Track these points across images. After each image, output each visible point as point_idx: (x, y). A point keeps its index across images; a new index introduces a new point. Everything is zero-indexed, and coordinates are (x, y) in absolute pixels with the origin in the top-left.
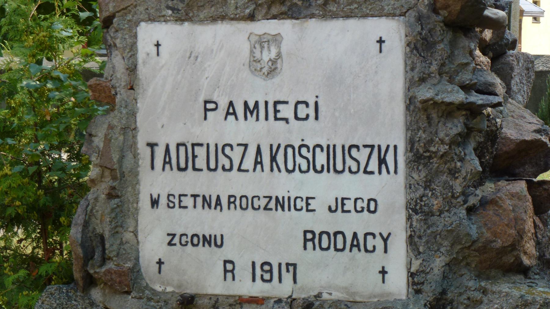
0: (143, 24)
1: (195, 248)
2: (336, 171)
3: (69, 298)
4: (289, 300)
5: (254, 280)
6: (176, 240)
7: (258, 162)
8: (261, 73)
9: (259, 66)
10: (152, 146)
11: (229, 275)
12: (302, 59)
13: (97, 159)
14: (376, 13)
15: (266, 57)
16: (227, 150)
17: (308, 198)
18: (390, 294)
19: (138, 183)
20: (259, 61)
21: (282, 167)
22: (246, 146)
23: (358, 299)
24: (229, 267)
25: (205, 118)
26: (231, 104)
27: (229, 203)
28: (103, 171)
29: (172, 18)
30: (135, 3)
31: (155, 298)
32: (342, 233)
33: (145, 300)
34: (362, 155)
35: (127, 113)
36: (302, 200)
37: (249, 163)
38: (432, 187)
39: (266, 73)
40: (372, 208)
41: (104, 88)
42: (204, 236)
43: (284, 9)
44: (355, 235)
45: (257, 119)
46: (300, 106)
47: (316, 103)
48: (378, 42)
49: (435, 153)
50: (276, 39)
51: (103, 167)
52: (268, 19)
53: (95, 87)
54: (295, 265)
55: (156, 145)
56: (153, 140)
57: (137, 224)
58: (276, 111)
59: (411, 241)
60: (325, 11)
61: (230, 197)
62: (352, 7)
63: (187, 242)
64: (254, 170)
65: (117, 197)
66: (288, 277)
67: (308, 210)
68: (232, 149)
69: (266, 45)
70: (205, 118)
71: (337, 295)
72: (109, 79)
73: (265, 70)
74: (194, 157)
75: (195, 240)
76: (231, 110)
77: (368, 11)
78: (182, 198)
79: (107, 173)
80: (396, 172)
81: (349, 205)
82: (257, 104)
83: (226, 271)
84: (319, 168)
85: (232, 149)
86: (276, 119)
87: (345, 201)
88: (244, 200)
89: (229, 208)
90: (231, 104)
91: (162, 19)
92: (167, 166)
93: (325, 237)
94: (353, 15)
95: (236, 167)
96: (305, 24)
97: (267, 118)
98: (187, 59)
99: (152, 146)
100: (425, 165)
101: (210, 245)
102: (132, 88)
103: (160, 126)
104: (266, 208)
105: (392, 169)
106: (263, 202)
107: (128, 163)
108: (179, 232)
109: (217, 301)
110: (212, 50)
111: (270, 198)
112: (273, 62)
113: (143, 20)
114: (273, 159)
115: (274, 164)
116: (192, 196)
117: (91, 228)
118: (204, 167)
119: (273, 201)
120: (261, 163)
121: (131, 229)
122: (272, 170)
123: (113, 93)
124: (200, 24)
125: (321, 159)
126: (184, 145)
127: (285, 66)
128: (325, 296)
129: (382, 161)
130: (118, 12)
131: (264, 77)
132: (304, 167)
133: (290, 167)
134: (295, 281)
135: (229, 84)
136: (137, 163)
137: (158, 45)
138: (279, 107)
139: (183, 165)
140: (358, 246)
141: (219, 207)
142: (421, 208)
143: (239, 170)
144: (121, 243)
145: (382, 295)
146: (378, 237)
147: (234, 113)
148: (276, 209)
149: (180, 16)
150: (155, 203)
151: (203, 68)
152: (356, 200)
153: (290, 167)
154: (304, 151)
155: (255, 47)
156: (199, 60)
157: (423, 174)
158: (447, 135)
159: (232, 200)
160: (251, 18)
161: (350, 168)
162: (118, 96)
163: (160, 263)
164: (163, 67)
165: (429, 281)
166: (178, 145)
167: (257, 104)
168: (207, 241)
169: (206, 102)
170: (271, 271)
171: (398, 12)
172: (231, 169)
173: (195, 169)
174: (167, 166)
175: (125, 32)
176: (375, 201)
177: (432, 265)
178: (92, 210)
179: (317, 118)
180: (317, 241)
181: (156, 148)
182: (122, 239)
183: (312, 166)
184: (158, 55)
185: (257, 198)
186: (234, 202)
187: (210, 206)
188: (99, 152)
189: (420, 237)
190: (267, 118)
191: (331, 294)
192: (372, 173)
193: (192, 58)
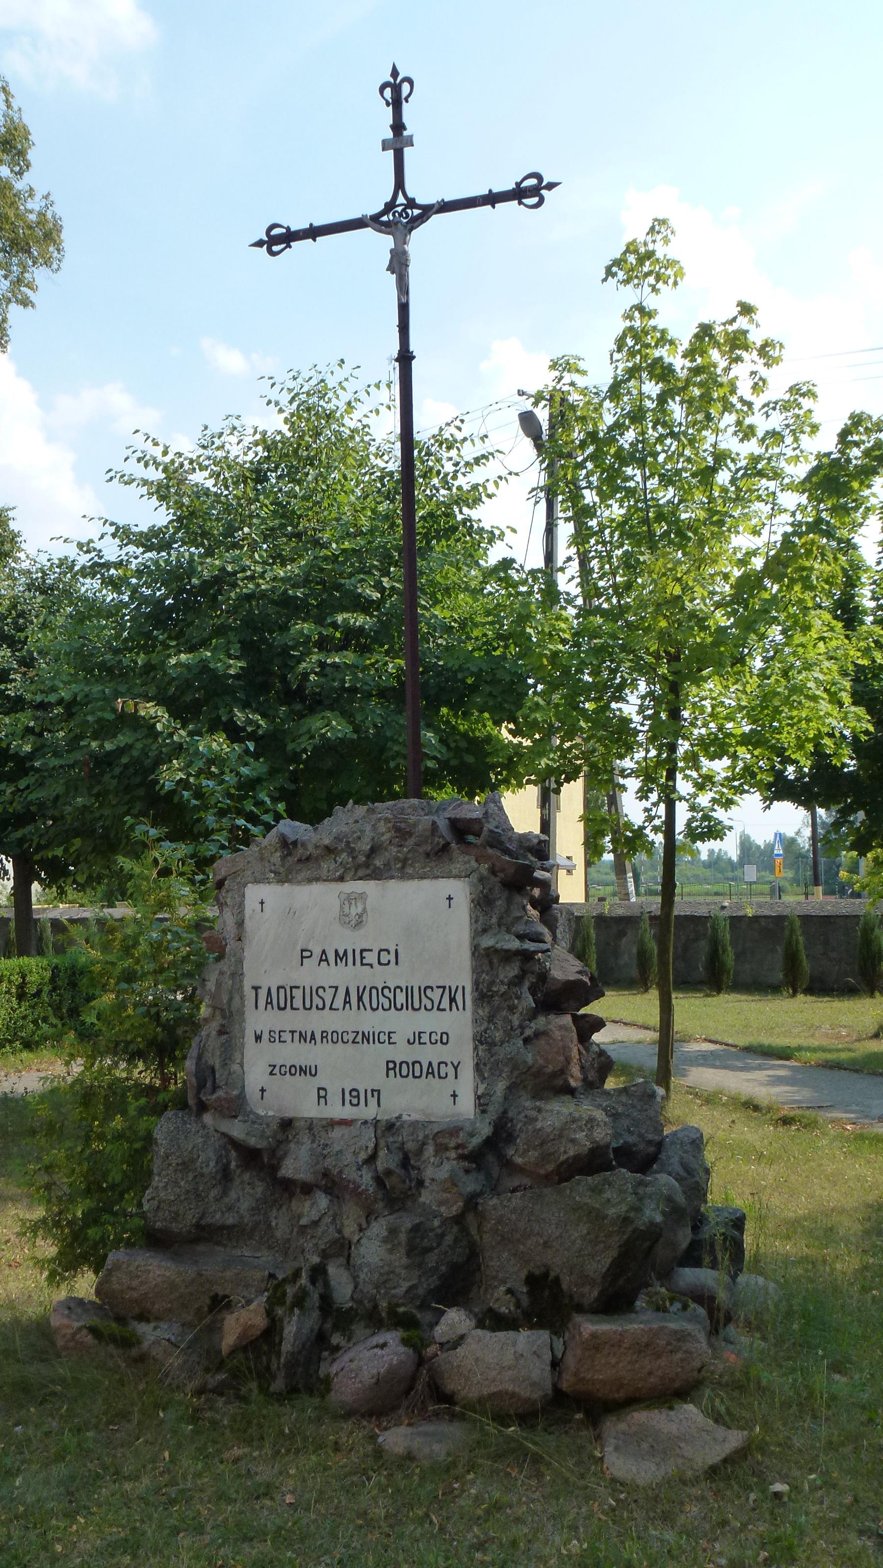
3: (185, 1123)
5: (343, 1104)
6: (277, 1071)
7: (347, 1002)
9: (347, 920)
10: (256, 989)
11: (322, 1100)
15: (354, 912)
16: (321, 991)
19: (244, 1021)
22: (336, 988)
23: (433, 1119)
24: (322, 1093)
26: (324, 952)
27: (322, 1037)
34: (436, 995)
37: (339, 1002)
40: (445, 1040)
43: (368, 872)
44: (430, 1064)
50: (362, 896)
51: (215, 1008)
59: (477, 1068)
61: (323, 1032)
66: (372, 1102)
71: (415, 1117)
73: (353, 923)
74: (292, 998)
76: (323, 958)
79: (218, 1013)
81: (425, 1038)
82: (345, 952)
83: (319, 1097)
84: (399, 1006)
86: (362, 964)
88: (335, 1035)
90: (324, 952)
92: (269, 1006)
93: (404, 1066)
99: (256, 989)
100: (489, 1002)
102: (240, 939)
104: (353, 1042)
106: (351, 1037)
108: (279, 1063)
109: (311, 1124)
112: (360, 916)
114: (360, 999)
118: (301, 1007)
120: (349, 1002)
125: (401, 998)
126: (283, 987)
129: (452, 1000)
137: (262, 903)
140: (433, 1073)
143: (331, 1008)
144: (230, 1074)
147: (326, 960)
150: (258, 1038)
160: (341, 879)
163: (263, 1090)
167: (345, 952)
168: (303, 1071)
169: (302, 951)
170: (358, 1097)
173: (292, 1008)
174: (269, 1006)
179: (397, 963)
183: (393, 1004)
189: (485, 1064)
192: (444, 1010)
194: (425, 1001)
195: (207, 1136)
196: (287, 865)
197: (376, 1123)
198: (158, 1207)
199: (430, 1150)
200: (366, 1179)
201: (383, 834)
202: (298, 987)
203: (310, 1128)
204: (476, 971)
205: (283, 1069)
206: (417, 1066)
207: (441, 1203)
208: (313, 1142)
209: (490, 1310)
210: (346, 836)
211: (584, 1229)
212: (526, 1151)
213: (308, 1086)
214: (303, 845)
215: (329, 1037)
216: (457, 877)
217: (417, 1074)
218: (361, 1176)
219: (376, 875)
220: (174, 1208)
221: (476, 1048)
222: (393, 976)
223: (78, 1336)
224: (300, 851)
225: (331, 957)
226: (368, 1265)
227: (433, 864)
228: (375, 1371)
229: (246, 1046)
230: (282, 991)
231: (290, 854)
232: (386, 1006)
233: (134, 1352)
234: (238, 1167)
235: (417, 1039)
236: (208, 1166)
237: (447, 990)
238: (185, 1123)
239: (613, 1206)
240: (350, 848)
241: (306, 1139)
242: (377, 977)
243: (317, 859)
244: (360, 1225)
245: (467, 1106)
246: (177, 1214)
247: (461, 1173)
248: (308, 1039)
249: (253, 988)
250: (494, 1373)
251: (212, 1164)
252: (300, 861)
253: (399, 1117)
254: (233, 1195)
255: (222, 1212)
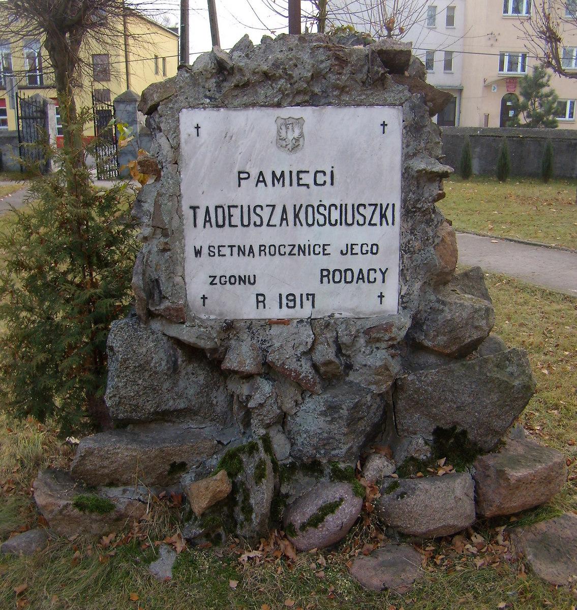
0: (184, 110)
1: (233, 286)
2: (347, 224)
3: (136, 330)
4: (309, 320)
5: (281, 307)
6: (217, 281)
7: (284, 219)
8: (287, 149)
9: (284, 143)
10: (194, 208)
11: (261, 305)
12: (321, 137)
13: (149, 221)
14: (381, 103)
15: (290, 136)
16: (258, 210)
17: (324, 245)
18: (384, 312)
19: (183, 238)
20: (285, 139)
21: (304, 222)
22: (274, 206)
23: (362, 316)
24: (261, 299)
25: (239, 186)
26: (261, 173)
27: (260, 251)
28: (155, 230)
29: (209, 106)
30: (175, 94)
31: (203, 325)
32: (351, 270)
33: (197, 327)
34: (368, 212)
35: (173, 183)
36: (320, 247)
37: (276, 220)
38: (415, 233)
39: (291, 149)
40: (374, 251)
41: (151, 163)
42: (240, 277)
43: (307, 98)
44: (361, 271)
45: (283, 185)
46: (318, 175)
47: (332, 172)
48: (381, 125)
49: (420, 209)
50: (300, 121)
51: (155, 227)
52: (292, 106)
53: (144, 163)
54: (313, 295)
55: (198, 207)
56: (195, 204)
57: (184, 269)
58: (299, 179)
59: (402, 273)
60: (340, 100)
61: (260, 246)
62: (361, 98)
63: (226, 282)
64: (281, 225)
65: (169, 250)
66: (308, 304)
67: (324, 254)
68: (262, 209)
69: (290, 126)
70: (239, 186)
71: (345, 314)
72: (156, 156)
73: (290, 147)
74: (230, 216)
75: (233, 280)
76: (261, 178)
77: (374, 101)
78: (221, 248)
79: (159, 231)
80: (393, 224)
81: (357, 249)
82: (283, 173)
83: (258, 302)
84: (333, 222)
85: (262, 209)
86: (299, 185)
87: (354, 246)
88: (272, 248)
89: (260, 255)
90: (261, 173)
91: (201, 106)
92: (208, 224)
93: (337, 273)
94: (362, 104)
95: (265, 223)
96: (324, 111)
97: (291, 185)
98: (223, 139)
99: (194, 208)
100: (411, 217)
101: (245, 284)
102: (176, 163)
103: (200, 193)
104: (290, 254)
105: (390, 221)
106: (288, 249)
107: (175, 223)
108: (219, 275)
109: (251, 324)
110: (245, 131)
111: (294, 246)
112: (297, 140)
113: (184, 108)
114: (296, 216)
115: (297, 220)
116: (229, 246)
117: (147, 275)
118: (239, 224)
119: (296, 249)
120: (286, 219)
121: (179, 274)
122: (295, 225)
123: (160, 167)
124: (234, 110)
125: (335, 215)
126: (221, 207)
127: (306, 142)
128: (337, 316)
129: (383, 216)
130: (162, 101)
131: (288, 152)
132: (322, 222)
133: (310, 221)
134: (313, 307)
135: (259, 157)
136: (182, 223)
137: (198, 127)
138: (301, 175)
139: (221, 223)
140: (363, 279)
141: (251, 255)
142: (408, 249)
143: (268, 225)
144: (174, 285)
145: (379, 313)
146: (378, 272)
147: (264, 181)
148: (299, 255)
149: (217, 104)
150: (198, 253)
151: (237, 146)
152: (362, 245)
153: (310, 221)
154: (322, 209)
155: (281, 129)
156: (233, 139)
157: (410, 224)
158: (431, 196)
159: (262, 248)
160: (279, 105)
161: (358, 221)
162: (164, 169)
163: (204, 298)
164: (201, 145)
165: (412, 300)
166: (216, 207)
167: (283, 173)
168: (242, 280)
169: (240, 173)
170: (294, 300)
171: (398, 103)
172: (261, 225)
173: (230, 225)
174: (208, 224)
175: (168, 118)
176: (377, 245)
177: (414, 289)
178: (147, 261)
179: (332, 184)
180: (331, 277)
181: (197, 210)
182: (173, 282)
183: (328, 221)
184: (198, 136)
185: (318, 246)
186: (264, 250)
187: (244, 254)
188: (150, 215)
189: (407, 270)
190: (291, 185)
191: (341, 314)
192: (375, 225)
193: (227, 138)
194: (357, 217)
195: (157, 340)
196: (224, 90)
197: (311, 321)
198: (120, 402)
199: (362, 341)
200: (305, 368)
201: (322, 62)
202: (236, 207)
203: (249, 328)
204: (405, 190)
205: (223, 279)
206: (349, 273)
207: (370, 383)
208: (252, 338)
209: (412, 458)
210: (282, 63)
211: (495, 397)
212: (436, 336)
213: (248, 294)
214: (240, 70)
215: (267, 250)
216: (392, 105)
217: (349, 279)
218: (301, 366)
219: (313, 100)
220: (134, 402)
221: (402, 257)
222: (328, 195)
223: (64, 512)
224: (238, 77)
225: (269, 179)
226: (307, 432)
227: (369, 92)
228: (339, 522)
229: (187, 260)
230: (220, 211)
231: (225, 80)
232: (322, 222)
233: (113, 515)
234: (183, 361)
235: (349, 250)
236: (161, 365)
237: (379, 207)
238: (136, 330)
239: (515, 378)
240: (286, 74)
241: (245, 336)
242: (315, 196)
243: (254, 85)
244: (296, 401)
245: (391, 303)
246: (137, 406)
247: (390, 358)
248: (247, 252)
249: (191, 207)
250: (438, 515)
251: (164, 363)
252: (237, 86)
253: (332, 316)
254: (182, 384)
255: (174, 399)
